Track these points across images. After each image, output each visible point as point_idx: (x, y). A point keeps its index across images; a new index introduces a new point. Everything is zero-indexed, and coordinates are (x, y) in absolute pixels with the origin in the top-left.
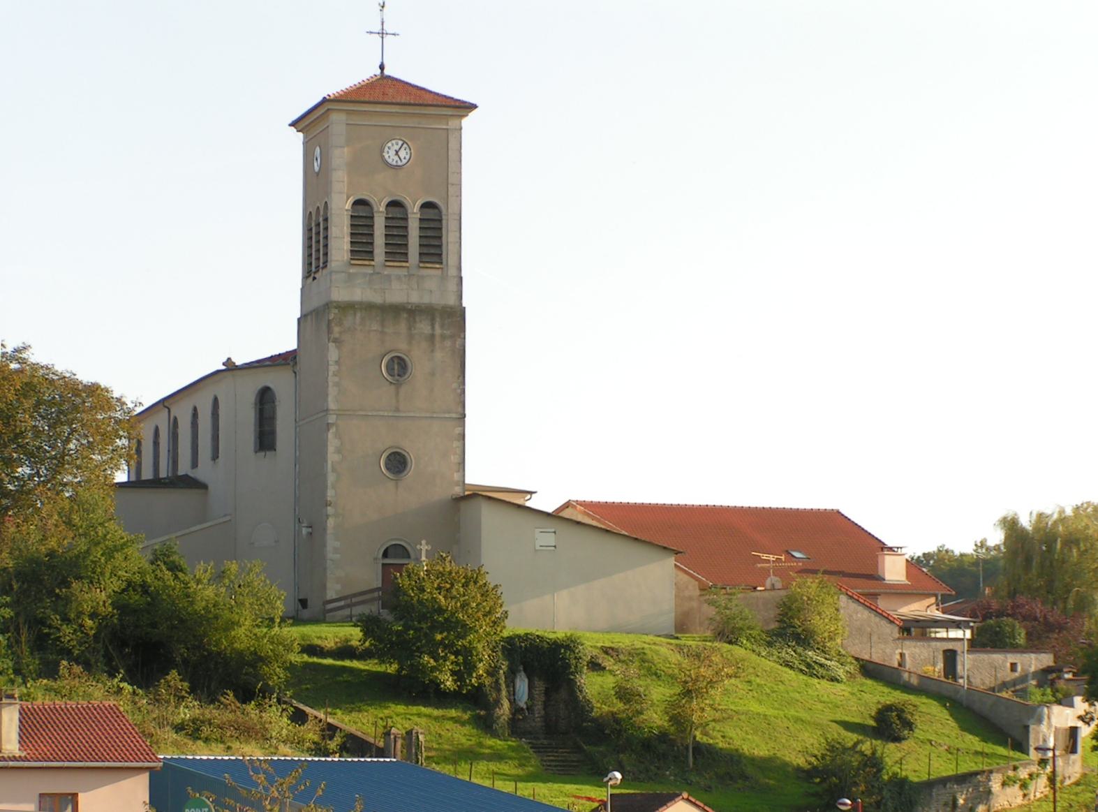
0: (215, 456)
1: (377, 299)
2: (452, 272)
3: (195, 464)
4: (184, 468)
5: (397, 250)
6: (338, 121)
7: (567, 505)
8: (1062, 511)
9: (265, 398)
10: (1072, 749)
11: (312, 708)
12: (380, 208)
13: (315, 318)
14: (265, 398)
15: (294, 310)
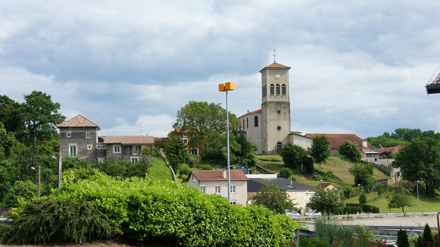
0: (248, 127)
1: (275, 101)
2: (288, 96)
3: (244, 129)
4: (242, 129)
5: (278, 93)
6: (268, 71)
7: (307, 134)
8: (45, 94)
9: (256, 118)
10: (399, 176)
11: (227, 159)
12: (281, 85)
13: (265, 104)
14: (256, 118)
15: (261, 103)
